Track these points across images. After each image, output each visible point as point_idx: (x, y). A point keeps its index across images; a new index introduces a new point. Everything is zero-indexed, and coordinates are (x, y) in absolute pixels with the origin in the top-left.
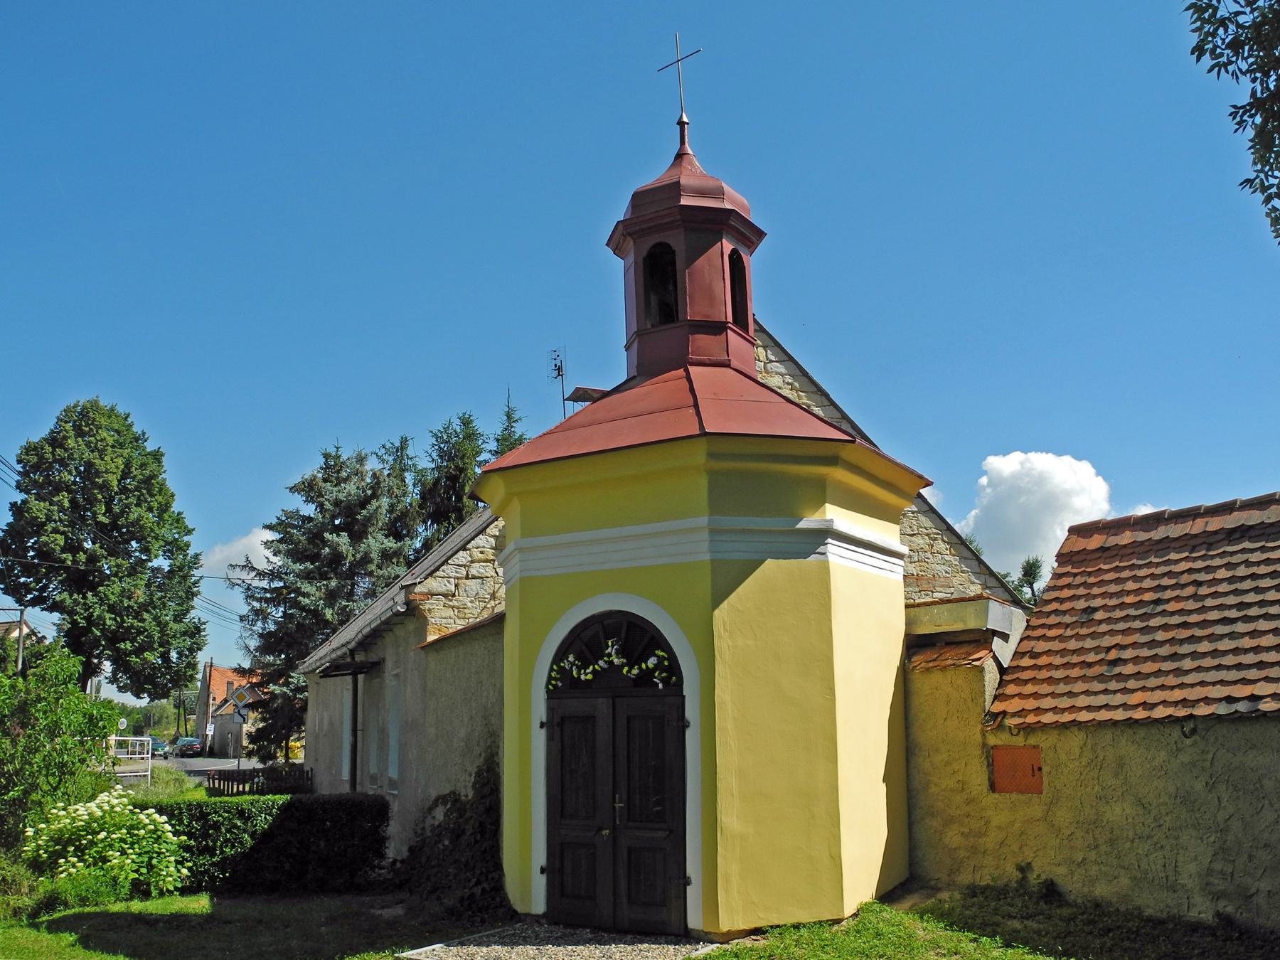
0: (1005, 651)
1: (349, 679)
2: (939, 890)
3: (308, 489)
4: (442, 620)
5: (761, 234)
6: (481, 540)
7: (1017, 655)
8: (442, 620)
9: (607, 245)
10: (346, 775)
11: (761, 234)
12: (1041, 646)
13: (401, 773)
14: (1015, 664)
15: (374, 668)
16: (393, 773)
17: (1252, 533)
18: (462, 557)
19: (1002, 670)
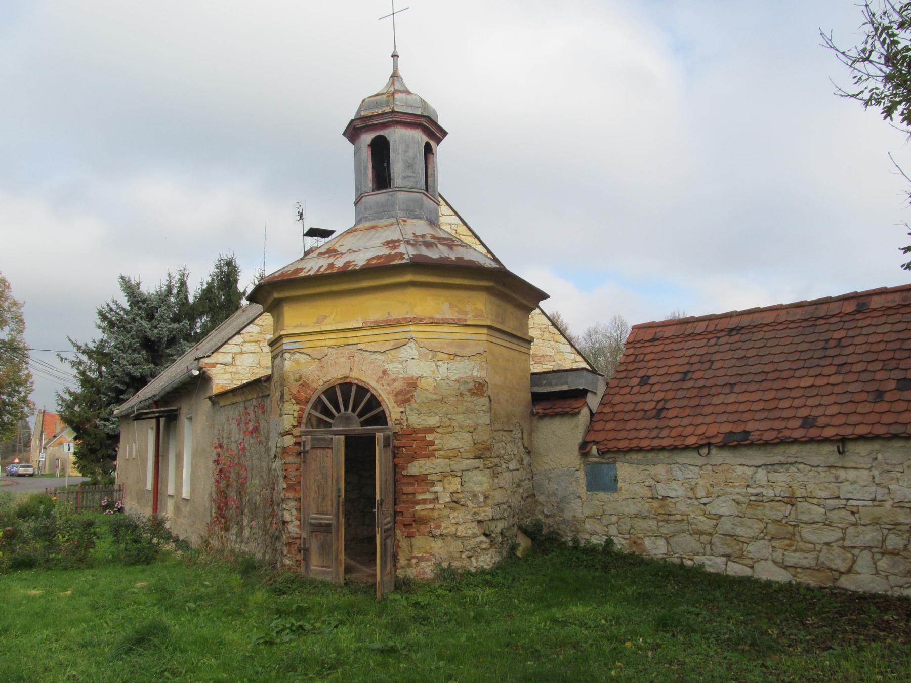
0: (593, 401)
1: (154, 421)
2: (433, 484)
3: (888, 112)
4: (222, 380)
5: (445, 133)
6: (251, 328)
7: (601, 404)
8: (222, 380)
9: (344, 134)
10: (150, 486)
11: (445, 133)
12: (617, 399)
13: (193, 491)
14: (277, 335)
15: (172, 418)
16: (186, 494)
17: (743, 331)
18: (238, 339)
19: (592, 414)
